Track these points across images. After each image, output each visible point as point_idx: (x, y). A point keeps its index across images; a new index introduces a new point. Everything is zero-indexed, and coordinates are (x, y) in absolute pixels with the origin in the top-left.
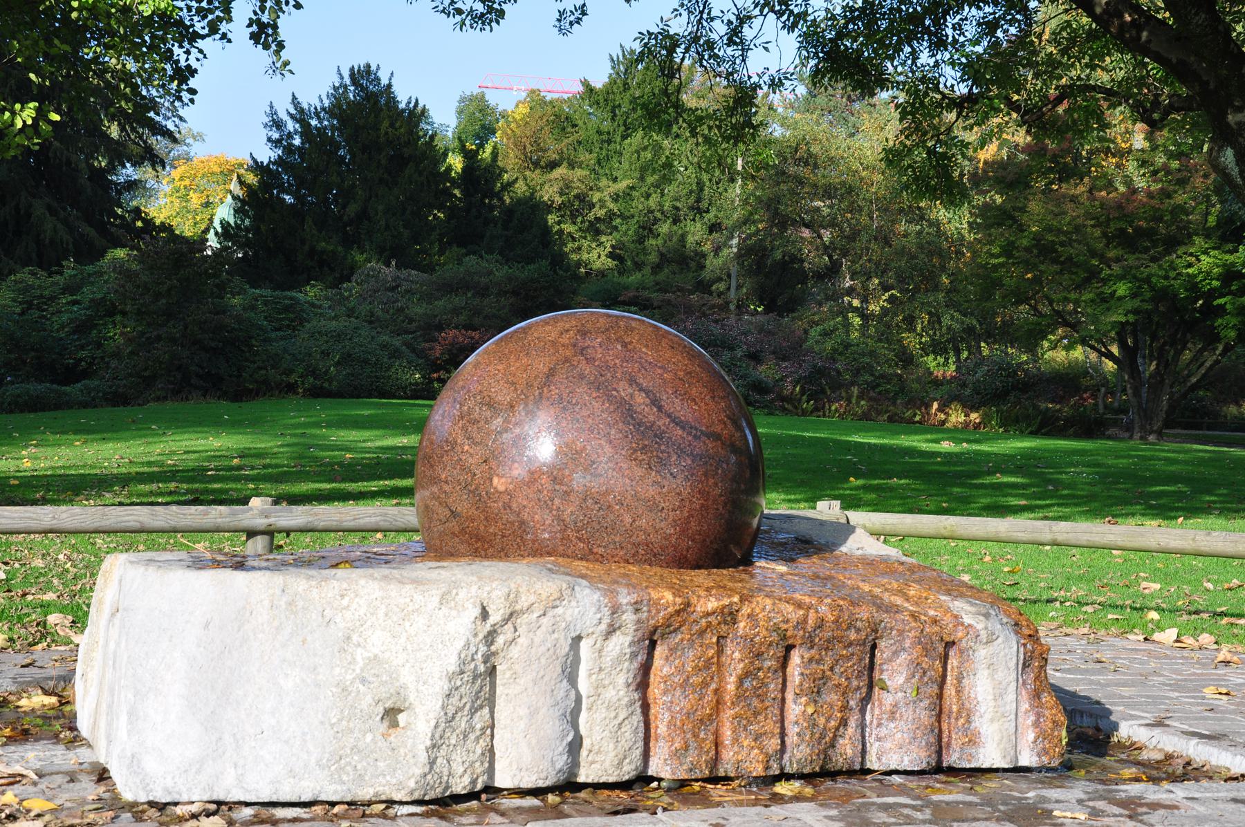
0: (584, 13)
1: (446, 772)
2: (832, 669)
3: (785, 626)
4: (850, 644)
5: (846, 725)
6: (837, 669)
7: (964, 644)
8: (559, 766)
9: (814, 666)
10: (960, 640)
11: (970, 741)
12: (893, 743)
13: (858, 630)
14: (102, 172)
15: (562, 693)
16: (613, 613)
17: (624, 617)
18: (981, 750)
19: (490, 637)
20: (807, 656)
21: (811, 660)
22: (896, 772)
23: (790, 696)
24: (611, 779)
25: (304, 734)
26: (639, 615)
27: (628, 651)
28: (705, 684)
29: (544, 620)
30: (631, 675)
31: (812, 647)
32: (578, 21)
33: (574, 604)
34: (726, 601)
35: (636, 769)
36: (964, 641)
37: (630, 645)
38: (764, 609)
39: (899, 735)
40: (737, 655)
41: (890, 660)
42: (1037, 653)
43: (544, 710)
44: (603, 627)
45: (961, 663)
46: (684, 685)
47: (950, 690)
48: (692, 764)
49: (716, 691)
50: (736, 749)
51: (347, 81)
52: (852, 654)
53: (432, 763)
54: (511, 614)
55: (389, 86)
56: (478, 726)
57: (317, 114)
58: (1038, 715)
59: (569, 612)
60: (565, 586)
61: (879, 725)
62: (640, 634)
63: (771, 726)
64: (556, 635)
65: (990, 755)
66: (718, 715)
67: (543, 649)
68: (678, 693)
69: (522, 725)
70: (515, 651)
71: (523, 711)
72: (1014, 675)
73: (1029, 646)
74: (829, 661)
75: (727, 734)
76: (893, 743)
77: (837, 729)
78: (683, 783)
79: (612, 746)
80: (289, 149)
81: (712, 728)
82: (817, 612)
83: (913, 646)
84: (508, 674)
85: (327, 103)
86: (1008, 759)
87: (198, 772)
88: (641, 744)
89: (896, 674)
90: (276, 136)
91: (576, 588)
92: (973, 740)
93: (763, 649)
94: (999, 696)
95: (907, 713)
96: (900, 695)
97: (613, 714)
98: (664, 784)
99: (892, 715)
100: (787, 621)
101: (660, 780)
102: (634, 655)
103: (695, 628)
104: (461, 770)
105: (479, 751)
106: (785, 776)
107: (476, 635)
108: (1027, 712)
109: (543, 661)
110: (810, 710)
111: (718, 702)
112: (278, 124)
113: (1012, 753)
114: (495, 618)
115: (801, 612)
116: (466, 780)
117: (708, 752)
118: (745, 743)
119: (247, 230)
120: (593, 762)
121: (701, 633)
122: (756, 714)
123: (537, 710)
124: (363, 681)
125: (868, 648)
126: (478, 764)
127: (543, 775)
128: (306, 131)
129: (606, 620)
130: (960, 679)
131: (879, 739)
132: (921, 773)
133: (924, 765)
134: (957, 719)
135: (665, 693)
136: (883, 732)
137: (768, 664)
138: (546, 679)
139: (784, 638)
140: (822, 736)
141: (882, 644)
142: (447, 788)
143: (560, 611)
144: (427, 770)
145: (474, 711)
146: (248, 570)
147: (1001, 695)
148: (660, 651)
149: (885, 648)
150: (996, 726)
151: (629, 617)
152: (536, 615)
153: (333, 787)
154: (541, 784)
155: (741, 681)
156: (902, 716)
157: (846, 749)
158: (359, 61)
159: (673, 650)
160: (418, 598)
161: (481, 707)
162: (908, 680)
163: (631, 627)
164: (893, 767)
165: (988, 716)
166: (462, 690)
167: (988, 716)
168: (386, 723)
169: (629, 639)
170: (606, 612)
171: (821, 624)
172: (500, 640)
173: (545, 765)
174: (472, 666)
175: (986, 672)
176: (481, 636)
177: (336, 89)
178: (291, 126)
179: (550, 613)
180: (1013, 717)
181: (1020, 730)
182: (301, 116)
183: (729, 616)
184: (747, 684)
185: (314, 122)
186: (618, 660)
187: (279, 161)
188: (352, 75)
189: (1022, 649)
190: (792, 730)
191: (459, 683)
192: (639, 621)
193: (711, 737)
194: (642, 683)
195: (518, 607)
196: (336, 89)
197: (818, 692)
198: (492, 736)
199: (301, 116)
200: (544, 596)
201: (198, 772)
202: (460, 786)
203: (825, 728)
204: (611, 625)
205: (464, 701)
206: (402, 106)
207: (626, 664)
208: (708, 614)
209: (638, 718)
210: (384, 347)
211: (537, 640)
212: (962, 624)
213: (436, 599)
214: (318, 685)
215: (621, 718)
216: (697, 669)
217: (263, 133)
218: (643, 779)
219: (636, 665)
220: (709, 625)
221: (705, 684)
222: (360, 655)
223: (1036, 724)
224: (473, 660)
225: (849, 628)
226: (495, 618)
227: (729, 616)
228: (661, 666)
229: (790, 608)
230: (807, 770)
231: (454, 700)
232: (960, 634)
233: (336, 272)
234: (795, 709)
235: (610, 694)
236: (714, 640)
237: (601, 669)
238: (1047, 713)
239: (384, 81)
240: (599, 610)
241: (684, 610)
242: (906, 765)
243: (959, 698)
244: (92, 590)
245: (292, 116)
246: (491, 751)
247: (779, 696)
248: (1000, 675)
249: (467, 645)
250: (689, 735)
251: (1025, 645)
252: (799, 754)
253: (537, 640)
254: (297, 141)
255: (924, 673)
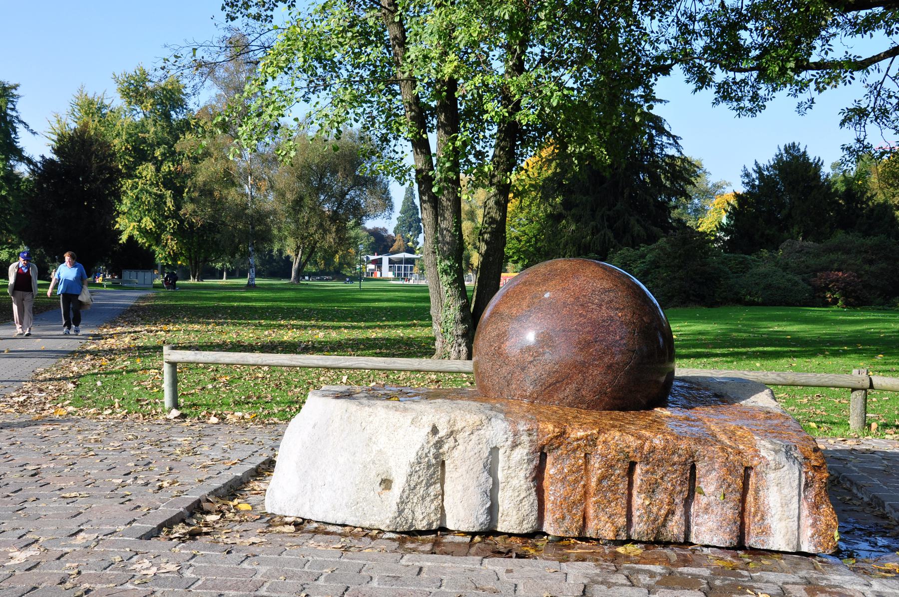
0: (813, 102)
1: (410, 517)
2: (662, 478)
3: (628, 450)
4: (674, 464)
5: (673, 513)
6: (666, 478)
7: (758, 469)
8: (481, 521)
9: (649, 475)
10: (756, 466)
11: (763, 532)
12: (709, 528)
13: (680, 456)
14: (664, 202)
15: (484, 480)
16: (515, 435)
17: (522, 438)
18: (771, 538)
19: (439, 444)
20: (645, 468)
21: (647, 472)
22: (707, 546)
23: (635, 492)
24: (516, 532)
25: (343, 488)
26: (531, 437)
27: (526, 458)
28: (576, 481)
29: (473, 437)
30: (528, 472)
31: (648, 464)
32: (810, 107)
33: (490, 428)
34: (589, 432)
35: (532, 527)
36: (758, 467)
37: (527, 454)
38: (613, 439)
39: (711, 523)
40: (597, 465)
41: (705, 476)
42: (817, 479)
43: (472, 489)
44: (509, 443)
45: (758, 481)
46: (563, 480)
47: (750, 498)
48: (569, 527)
49: (584, 486)
50: (596, 521)
51: (783, 152)
52: (676, 470)
53: (400, 512)
54: (452, 432)
55: (805, 152)
56: (432, 494)
57: (767, 169)
58: (815, 520)
59: (488, 433)
60: (484, 417)
61: (697, 516)
62: (533, 448)
63: (621, 510)
64: (481, 446)
65: (778, 541)
66: (586, 500)
67: (473, 453)
68: (559, 485)
69: (459, 495)
70: (456, 453)
71: (460, 488)
72: (796, 492)
73: (810, 474)
74: (660, 473)
75: (591, 512)
76: (709, 528)
77: (667, 516)
78: (561, 539)
79: (515, 512)
80: (753, 186)
81: (581, 508)
82: (652, 442)
83: (720, 468)
84: (452, 466)
85: (772, 163)
86: (791, 546)
87: (295, 501)
88: (535, 513)
89: (709, 484)
90: (746, 181)
91: (493, 420)
92: (765, 531)
93: (614, 463)
94: (785, 504)
95: (717, 510)
96: (713, 498)
97: (517, 494)
98: (550, 538)
99: (706, 510)
100: (629, 447)
101: (548, 535)
102: (530, 461)
103: (570, 447)
104: (421, 517)
105: (433, 507)
106: (629, 541)
107: (428, 442)
108: (807, 516)
109: (472, 460)
110: (647, 502)
111: (585, 493)
112: (747, 175)
113: (795, 542)
114: (442, 433)
115: (639, 442)
116: (425, 523)
117: (578, 522)
118: (603, 519)
119: (732, 226)
120: (504, 521)
121: (574, 450)
122: (610, 502)
123: (468, 488)
124: (374, 463)
125: (688, 467)
126: (432, 515)
127: (472, 525)
128: (761, 176)
129: (511, 439)
130: (757, 491)
131: (697, 525)
132: (728, 548)
133: (728, 544)
134: (754, 517)
135: (552, 484)
136: (700, 520)
137: (618, 472)
138: (474, 470)
139: (628, 457)
140: (655, 520)
141: (699, 465)
142: (412, 525)
143: (482, 432)
144: (396, 514)
145: (428, 485)
146: (354, 399)
147: (786, 504)
148: (550, 459)
149: (701, 468)
150: (783, 523)
151: (525, 438)
152: (468, 433)
153: (352, 518)
154: (471, 530)
155: (600, 481)
156: (713, 511)
157: (674, 528)
158: (789, 142)
159: (556, 459)
160: (401, 419)
161: (435, 483)
162: (717, 489)
163: (527, 444)
164: (706, 543)
165: (777, 517)
166: (420, 473)
167: (777, 517)
168: (383, 486)
169: (526, 451)
170: (511, 434)
171: (653, 450)
172: (446, 447)
173: (473, 519)
174: (427, 459)
175: (776, 488)
176: (432, 443)
177: (777, 156)
178: (754, 175)
179: (476, 433)
180: (796, 519)
181: (802, 527)
182: (759, 170)
183: (592, 441)
184: (605, 483)
185: (766, 173)
186: (520, 463)
187: (748, 193)
188: (786, 149)
189: (803, 475)
190: (636, 513)
191: (418, 469)
192: (531, 441)
193: (580, 514)
194: (538, 475)
195: (455, 428)
196: (777, 156)
197: (653, 492)
198: (443, 500)
199: (759, 170)
200: (471, 423)
201: (295, 501)
202: (421, 525)
203: (657, 514)
204: (513, 442)
205: (421, 479)
206: (811, 161)
207: (525, 466)
208: (578, 440)
209: (533, 497)
210: (789, 280)
211: (469, 448)
212: (758, 456)
213: (410, 420)
214: (354, 463)
215: (522, 497)
216: (571, 472)
217: (740, 180)
218: (537, 533)
219: (532, 466)
220: (579, 446)
221: (576, 481)
222: (375, 448)
223: (813, 525)
224: (427, 456)
225: (673, 453)
226: (442, 433)
227: (592, 441)
228: (550, 470)
229: (631, 439)
230: (644, 539)
231: (415, 478)
232: (755, 462)
233: (773, 244)
234: (638, 500)
235: (515, 482)
236: (583, 455)
237: (509, 467)
238: (822, 518)
239: (802, 150)
240: (505, 433)
241: (561, 436)
242: (715, 542)
243: (756, 504)
244: (304, 402)
245: (755, 171)
246: (442, 508)
247: (626, 492)
248: (786, 491)
249: (423, 448)
250: (565, 511)
251: (806, 473)
252: (639, 528)
253: (469, 448)
254: (757, 183)
255: (729, 486)
